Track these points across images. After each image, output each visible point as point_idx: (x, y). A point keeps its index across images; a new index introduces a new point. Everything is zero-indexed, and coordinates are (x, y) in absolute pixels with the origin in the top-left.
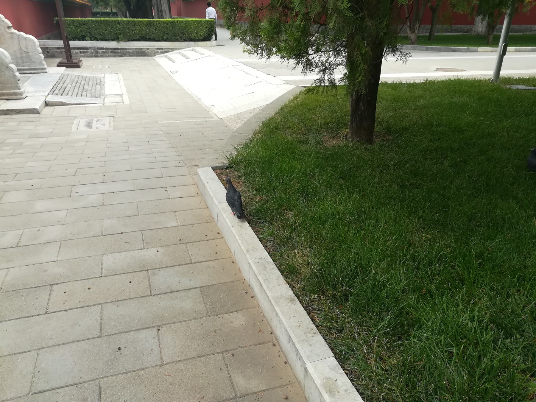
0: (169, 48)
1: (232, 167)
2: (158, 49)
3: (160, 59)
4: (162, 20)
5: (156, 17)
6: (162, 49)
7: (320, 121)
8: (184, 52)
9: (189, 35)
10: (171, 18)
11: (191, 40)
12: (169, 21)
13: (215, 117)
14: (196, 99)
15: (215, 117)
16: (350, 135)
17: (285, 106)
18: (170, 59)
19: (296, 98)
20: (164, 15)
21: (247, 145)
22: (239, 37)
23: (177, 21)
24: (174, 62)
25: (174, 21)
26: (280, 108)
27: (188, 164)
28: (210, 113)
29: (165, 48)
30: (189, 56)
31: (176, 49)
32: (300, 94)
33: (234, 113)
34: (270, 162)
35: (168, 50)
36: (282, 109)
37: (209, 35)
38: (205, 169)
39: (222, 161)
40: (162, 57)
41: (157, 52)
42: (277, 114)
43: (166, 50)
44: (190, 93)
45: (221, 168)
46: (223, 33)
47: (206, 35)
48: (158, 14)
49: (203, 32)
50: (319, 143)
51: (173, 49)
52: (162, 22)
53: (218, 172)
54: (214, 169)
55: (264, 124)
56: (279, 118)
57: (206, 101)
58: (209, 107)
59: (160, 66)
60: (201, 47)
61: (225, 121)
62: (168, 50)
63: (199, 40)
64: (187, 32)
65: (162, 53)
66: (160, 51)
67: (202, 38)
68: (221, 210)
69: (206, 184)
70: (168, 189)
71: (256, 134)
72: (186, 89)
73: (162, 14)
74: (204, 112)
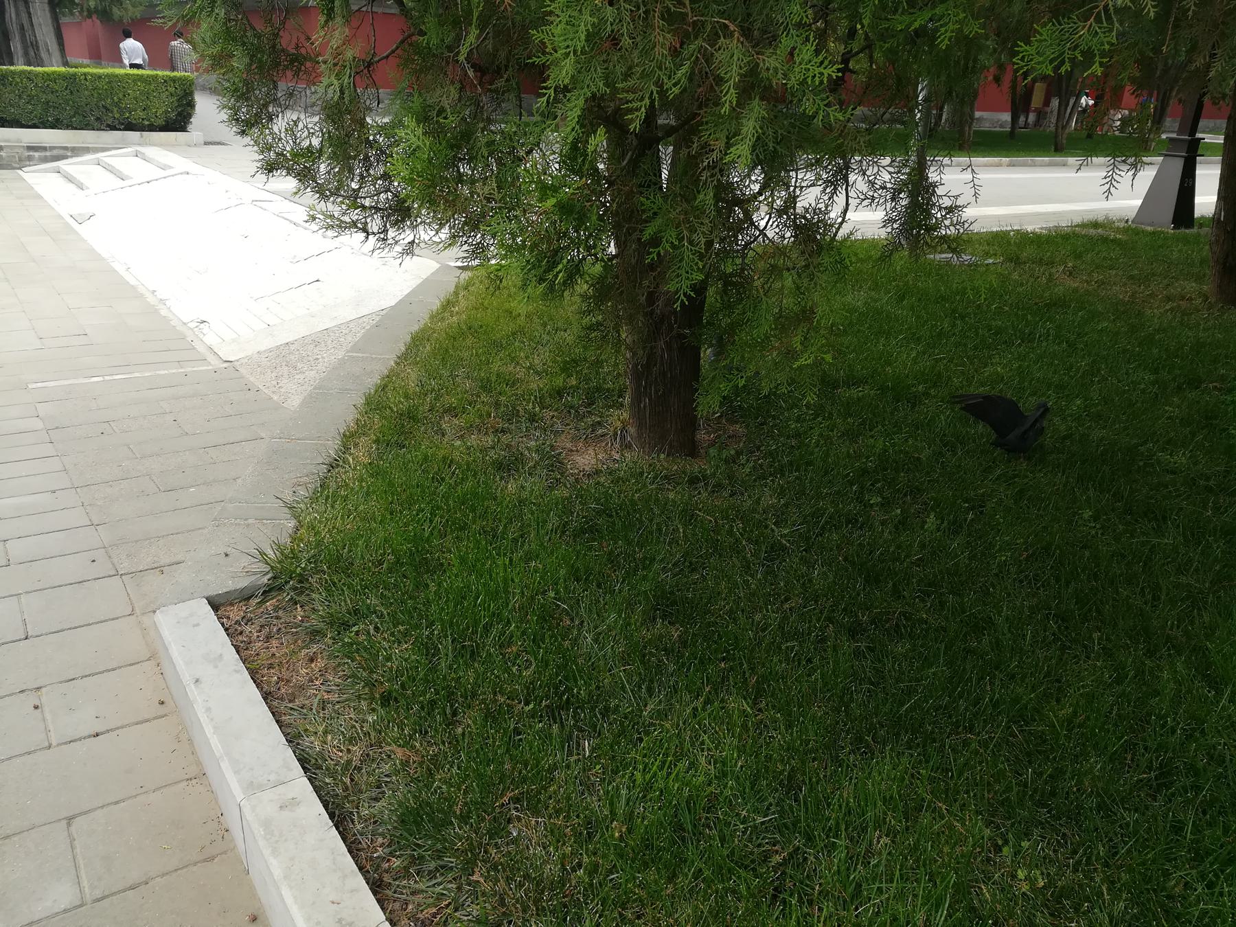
0: (66, 148)
1: (280, 589)
2: (30, 148)
3: (40, 179)
4: (39, 69)
5: (21, 60)
6: (45, 149)
7: (535, 384)
8: (108, 160)
9: (121, 112)
10: (66, 64)
11: (130, 127)
12: (59, 75)
13: (211, 358)
14: (151, 299)
15: (211, 358)
16: (632, 430)
17: (423, 330)
18: (70, 179)
19: (448, 305)
20: (44, 55)
21: (326, 490)
22: (289, 171)
23: (85, 74)
24: (81, 187)
25: (75, 75)
26: (408, 338)
27: (125, 566)
28: (196, 344)
29: (52, 148)
30: (126, 172)
31: (87, 150)
32: (456, 293)
33: (267, 343)
34: (421, 564)
35: (61, 152)
36: (418, 340)
37: (179, 114)
38: (183, 609)
39: (240, 573)
40: (46, 171)
41: (30, 158)
42: (403, 359)
43: (55, 152)
44: (133, 282)
45: (245, 596)
46: (209, 110)
47: (173, 115)
48: (26, 54)
49: (163, 106)
50: (555, 463)
51: (76, 151)
52: (37, 75)
53: (235, 613)
54: (215, 604)
55: (368, 402)
56: (413, 376)
57: (183, 309)
58: (192, 325)
59: (39, 197)
60: (160, 145)
61: (242, 370)
62: (61, 152)
63: (152, 128)
64: (117, 105)
65: (45, 160)
66: (36, 154)
67: (161, 122)
68: (259, 831)
69: (192, 690)
70: (46, 698)
71: (349, 439)
72: (121, 270)
73: (37, 55)
74: (174, 342)
